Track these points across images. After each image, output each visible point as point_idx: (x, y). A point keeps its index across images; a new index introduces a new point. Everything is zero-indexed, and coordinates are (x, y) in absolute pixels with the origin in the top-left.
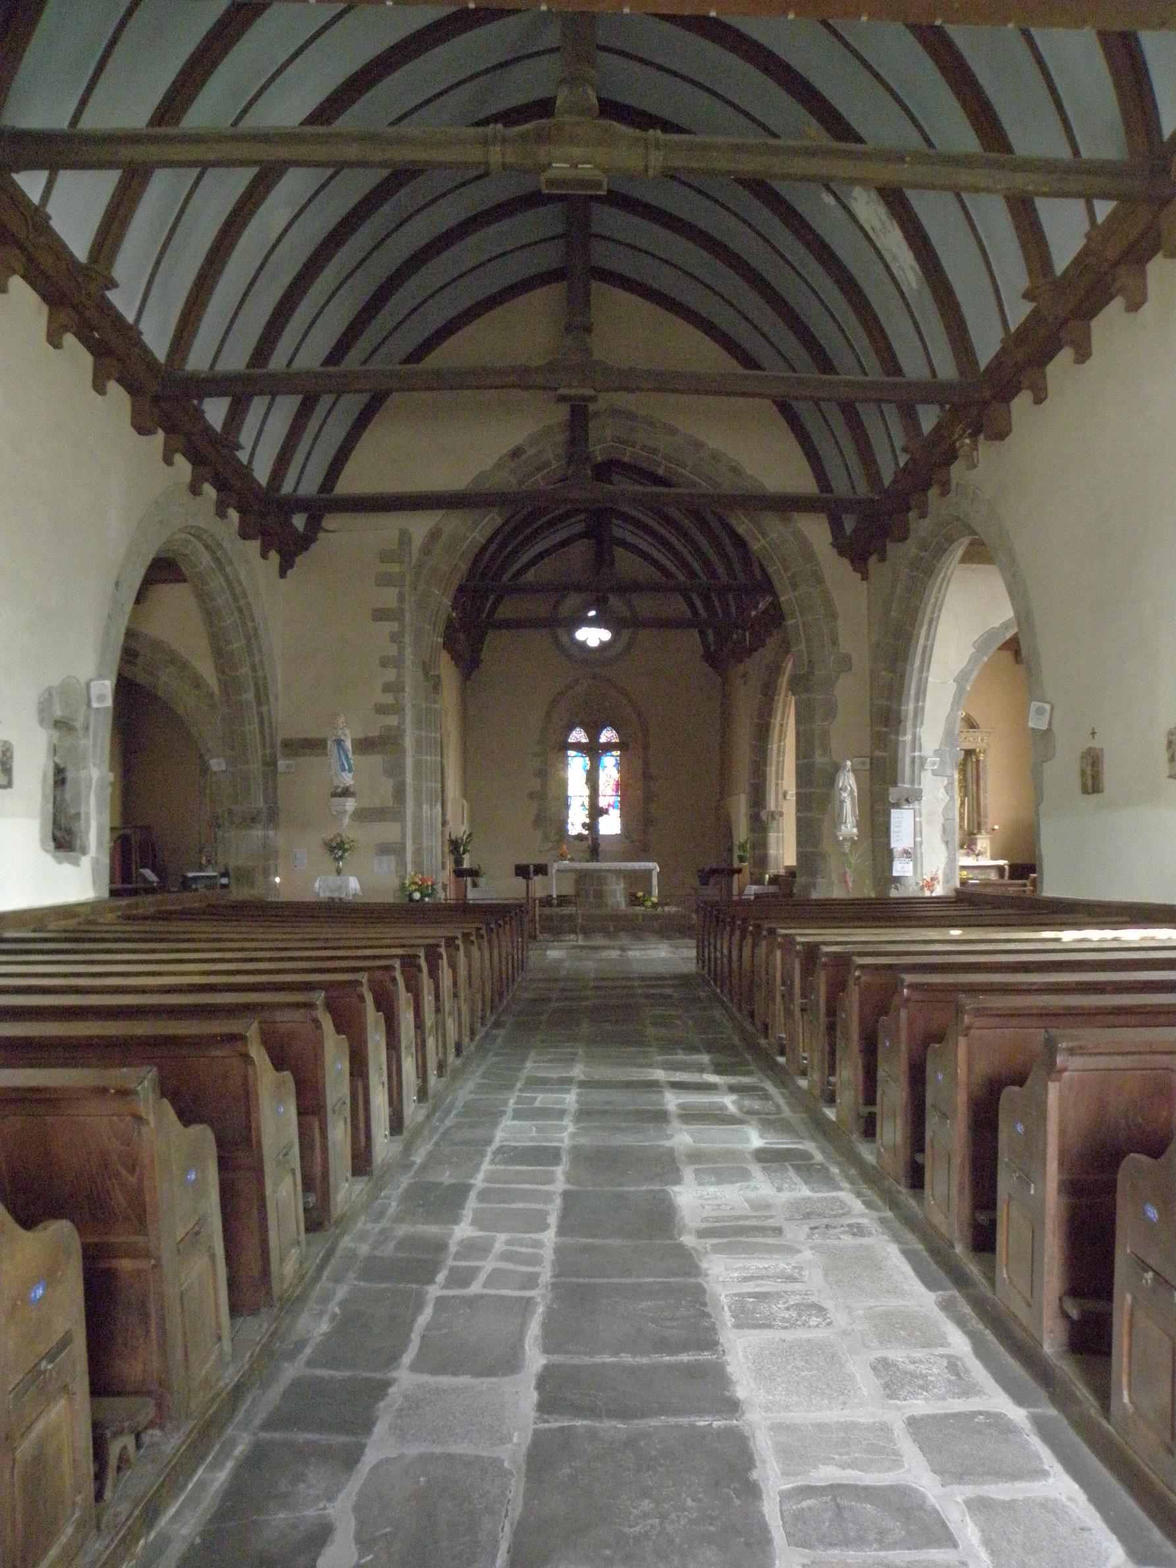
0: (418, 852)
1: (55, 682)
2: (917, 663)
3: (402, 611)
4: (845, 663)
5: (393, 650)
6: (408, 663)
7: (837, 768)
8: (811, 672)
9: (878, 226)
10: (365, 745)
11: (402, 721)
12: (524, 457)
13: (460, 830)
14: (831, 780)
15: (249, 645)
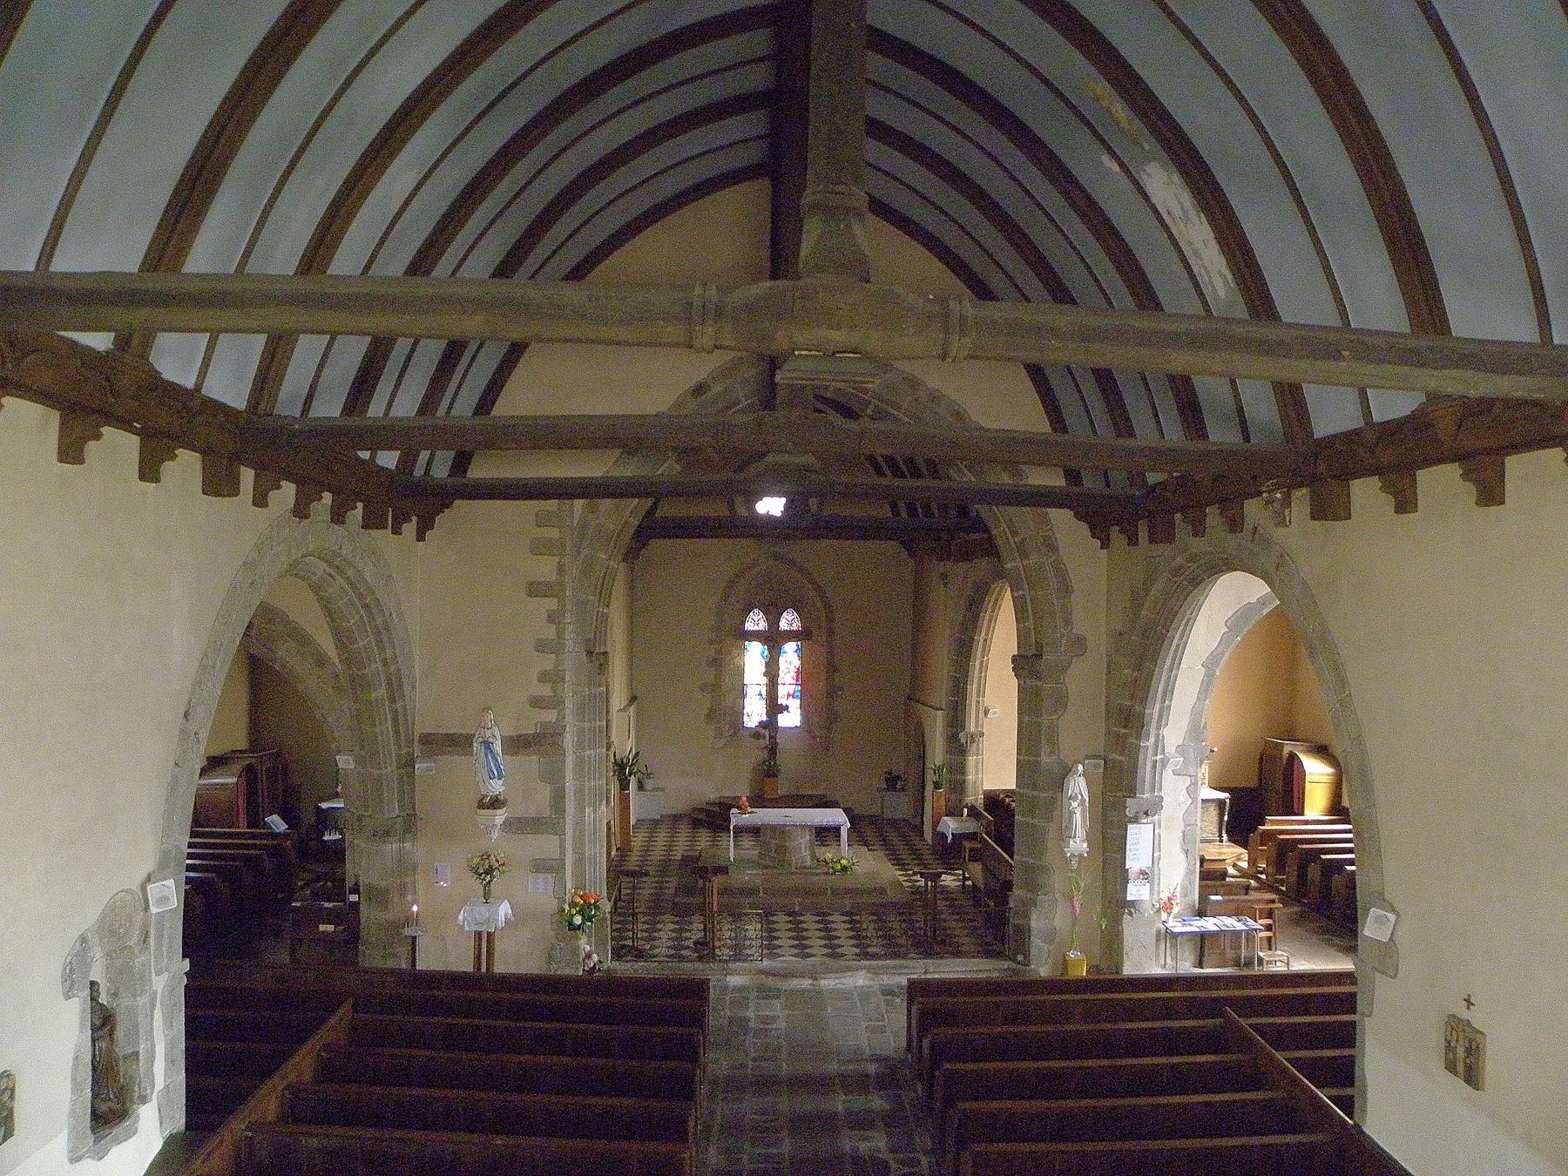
0: (579, 862)
1: (91, 915)
2: (1168, 663)
3: (561, 584)
4: (1080, 644)
5: (550, 632)
6: (569, 644)
7: (1067, 771)
8: (1039, 656)
9: (1178, 212)
10: (517, 744)
11: (561, 716)
12: (709, 394)
13: (625, 745)
14: (1060, 785)
15: (379, 642)
